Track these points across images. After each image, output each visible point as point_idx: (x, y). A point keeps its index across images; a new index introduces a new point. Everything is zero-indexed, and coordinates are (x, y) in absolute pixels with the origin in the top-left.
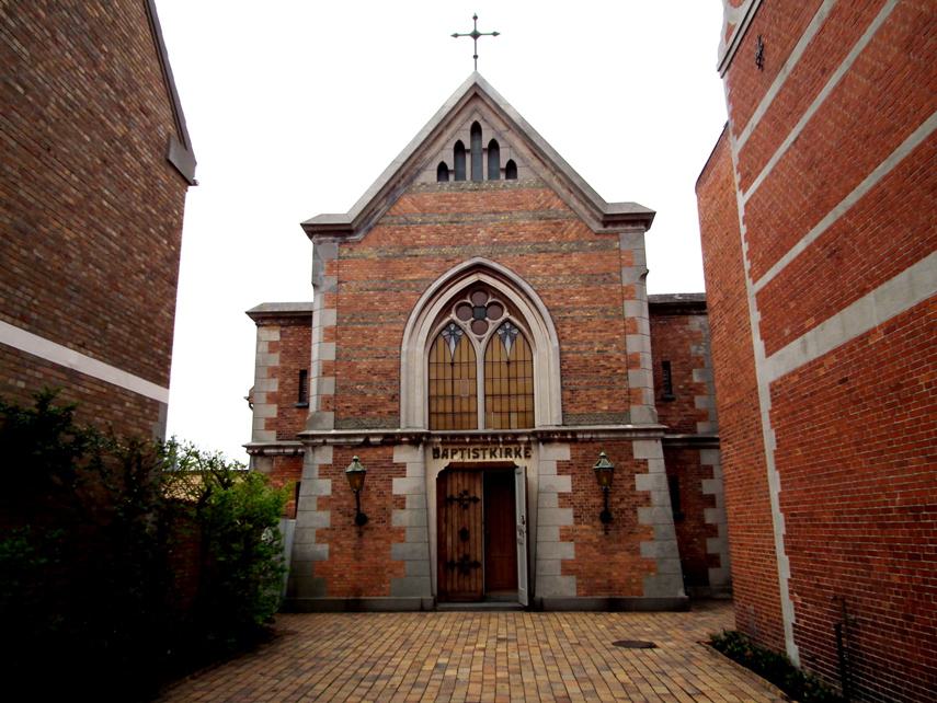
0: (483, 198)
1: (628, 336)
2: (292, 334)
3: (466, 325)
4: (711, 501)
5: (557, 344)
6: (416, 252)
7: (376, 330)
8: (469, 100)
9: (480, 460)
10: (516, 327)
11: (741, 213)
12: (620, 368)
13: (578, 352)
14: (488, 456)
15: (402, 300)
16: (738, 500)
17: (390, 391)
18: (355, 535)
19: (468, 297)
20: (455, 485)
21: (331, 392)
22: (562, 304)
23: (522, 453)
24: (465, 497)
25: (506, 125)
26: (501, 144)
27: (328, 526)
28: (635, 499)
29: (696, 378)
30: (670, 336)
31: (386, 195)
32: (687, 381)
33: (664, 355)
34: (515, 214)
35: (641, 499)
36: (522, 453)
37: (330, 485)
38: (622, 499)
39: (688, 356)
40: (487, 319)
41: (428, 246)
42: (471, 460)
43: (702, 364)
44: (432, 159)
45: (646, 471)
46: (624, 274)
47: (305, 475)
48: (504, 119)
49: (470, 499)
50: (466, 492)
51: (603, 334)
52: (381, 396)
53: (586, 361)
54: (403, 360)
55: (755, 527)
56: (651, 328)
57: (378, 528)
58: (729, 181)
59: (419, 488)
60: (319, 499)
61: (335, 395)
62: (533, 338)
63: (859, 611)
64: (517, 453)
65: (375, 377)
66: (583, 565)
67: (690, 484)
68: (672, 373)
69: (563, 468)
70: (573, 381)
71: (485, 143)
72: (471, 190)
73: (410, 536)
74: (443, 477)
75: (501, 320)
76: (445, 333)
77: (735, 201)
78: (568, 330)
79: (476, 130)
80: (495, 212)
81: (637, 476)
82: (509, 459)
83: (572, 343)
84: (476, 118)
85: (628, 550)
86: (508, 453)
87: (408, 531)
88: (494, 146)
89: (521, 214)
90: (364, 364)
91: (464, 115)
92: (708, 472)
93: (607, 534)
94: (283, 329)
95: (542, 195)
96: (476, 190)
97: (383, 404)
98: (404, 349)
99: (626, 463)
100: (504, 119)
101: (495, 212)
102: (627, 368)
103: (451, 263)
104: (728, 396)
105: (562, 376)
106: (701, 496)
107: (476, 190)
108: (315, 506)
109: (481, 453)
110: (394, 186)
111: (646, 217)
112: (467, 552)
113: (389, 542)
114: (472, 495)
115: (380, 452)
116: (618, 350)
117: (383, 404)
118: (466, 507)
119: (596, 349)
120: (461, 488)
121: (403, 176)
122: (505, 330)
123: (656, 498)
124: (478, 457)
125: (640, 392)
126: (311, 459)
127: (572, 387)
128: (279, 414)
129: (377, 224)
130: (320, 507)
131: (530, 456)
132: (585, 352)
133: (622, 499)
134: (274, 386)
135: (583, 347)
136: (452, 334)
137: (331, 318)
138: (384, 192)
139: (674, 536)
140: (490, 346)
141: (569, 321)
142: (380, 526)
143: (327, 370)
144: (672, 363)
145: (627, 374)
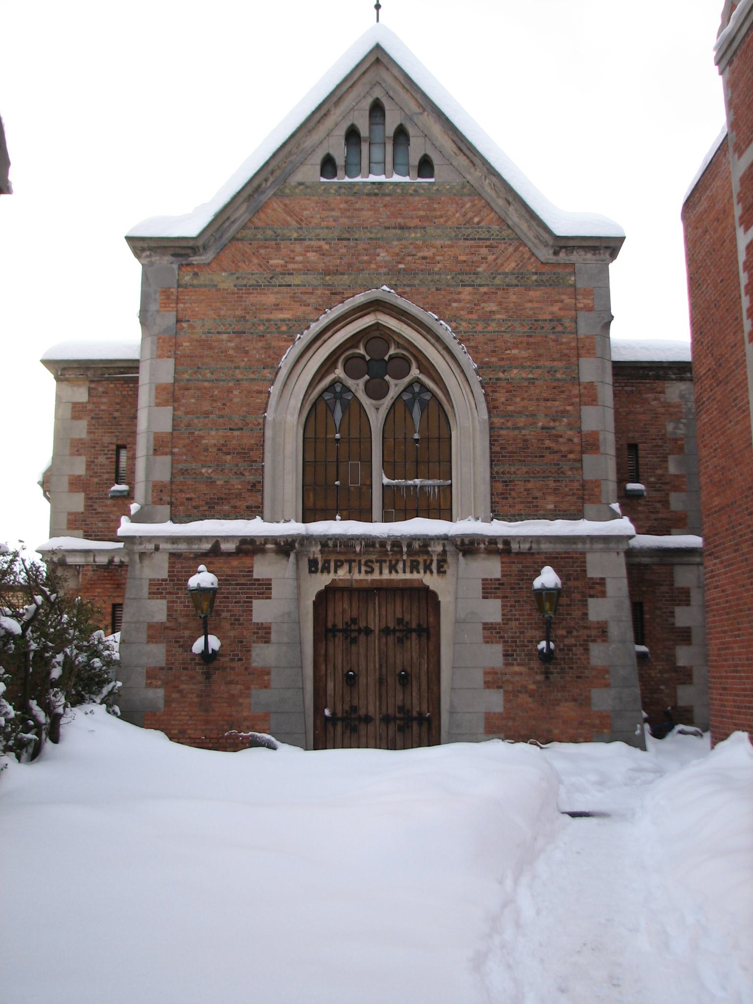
0: (385, 206)
1: (584, 408)
2: (105, 392)
3: (358, 386)
4: (685, 636)
5: (486, 417)
6: (288, 279)
7: (230, 391)
8: (368, 69)
9: (376, 576)
10: (428, 390)
11: (742, 257)
12: (571, 452)
13: (516, 428)
14: (386, 571)
15: (268, 348)
16: (725, 632)
17: (250, 478)
18: (200, 678)
19: (361, 346)
20: (339, 609)
21: (166, 477)
22: (494, 360)
23: (434, 567)
24: (353, 627)
25: (420, 106)
26: (411, 131)
27: (163, 664)
28: (586, 632)
29: (673, 468)
30: (638, 408)
31: (250, 196)
32: (659, 472)
33: (630, 435)
34: (430, 230)
35: (594, 633)
36: (434, 567)
37: (165, 608)
38: (569, 632)
39: (663, 438)
40: (387, 378)
41: (307, 271)
42: (363, 576)
43: (681, 449)
44: (313, 150)
45: (603, 594)
46: (582, 324)
47: (130, 593)
48: (418, 97)
49: (359, 631)
50: (354, 621)
51: (549, 404)
52: (237, 485)
53: (526, 441)
54: (269, 433)
55: (743, 666)
56: (615, 395)
57: (233, 669)
58: (727, 212)
59: (289, 614)
60: (151, 626)
61: (172, 482)
62: (453, 407)
63: (740, 668)
64: (428, 568)
65: (229, 457)
66: (514, 719)
67: (658, 612)
68: (641, 461)
69: (489, 589)
70: (506, 468)
71: (390, 128)
72: (368, 195)
73: (275, 679)
74: (324, 598)
75: (407, 380)
76: (327, 396)
77: (733, 240)
78: (501, 397)
79: (377, 109)
80: (401, 228)
81: (591, 601)
82: (415, 576)
83: (508, 415)
84: (378, 93)
85: (575, 700)
86: (414, 567)
87: (274, 673)
88: (401, 134)
89: (439, 231)
90: (212, 438)
91: (359, 90)
92: (683, 597)
93: (547, 678)
94: (93, 385)
95: (468, 205)
96: (376, 195)
97: (239, 496)
98: (270, 415)
99: (577, 583)
100: (418, 97)
101: (401, 228)
102: (582, 452)
103: (339, 297)
104: (717, 495)
105: (492, 461)
106: (673, 629)
107: (376, 195)
108: (144, 636)
109: (376, 566)
110: (259, 186)
111: (612, 244)
112: (355, 703)
113: (248, 688)
114: (362, 624)
115: (235, 563)
116: (570, 426)
117: (239, 496)
118: (354, 641)
119: (540, 424)
120: (347, 618)
121: (272, 172)
122: (413, 393)
123: (614, 631)
124: (372, 571)
125: (599, 486)
126: (137, 572)
127: (506, 477)
128: (87, 506)
129: (234, 239)
130: (151, 639)
131: (445, 572)
132: (524, 428)
133: (569, 632)
134: (80, 468)
135: (521, 421)
136: (338, 397)
137: (166, 372)
138: (245, 194)
139: (637, 682)
140: (392, 411)
141: (504, 384)
142: (233, 665)
143: (160, 446)
144: (641, 446)
145: (581, 460)
